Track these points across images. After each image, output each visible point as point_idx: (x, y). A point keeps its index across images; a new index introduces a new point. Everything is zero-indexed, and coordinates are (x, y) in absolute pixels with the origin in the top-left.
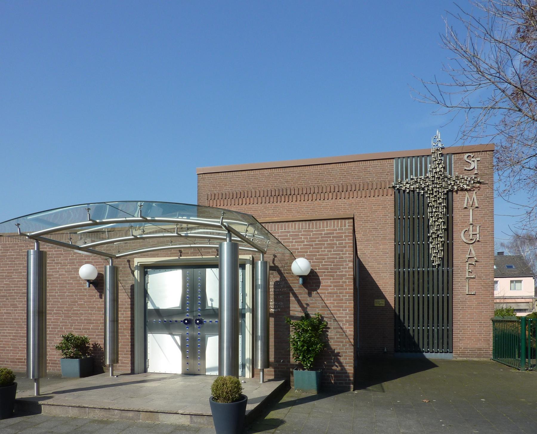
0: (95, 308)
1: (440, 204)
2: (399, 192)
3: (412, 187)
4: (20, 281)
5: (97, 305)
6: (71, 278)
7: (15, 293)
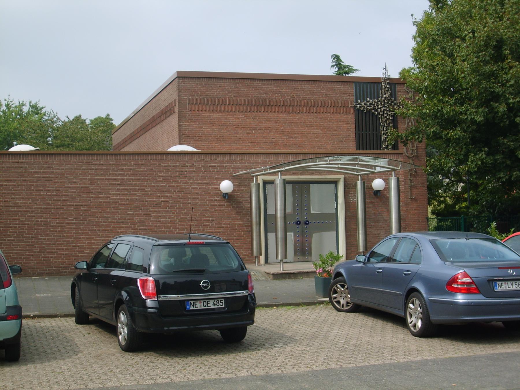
0: (224, 215)
1: (389, 123)
2: (358, 111)
3: (369, 108)
4: (154, 194)
5: (226, 212)
6: (203, 191)
7: (148, 204)
